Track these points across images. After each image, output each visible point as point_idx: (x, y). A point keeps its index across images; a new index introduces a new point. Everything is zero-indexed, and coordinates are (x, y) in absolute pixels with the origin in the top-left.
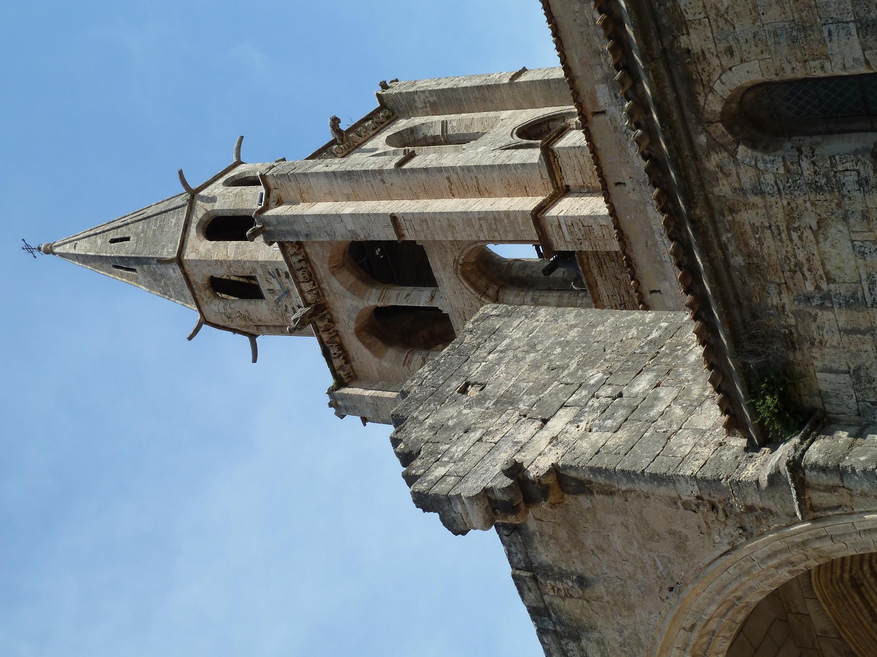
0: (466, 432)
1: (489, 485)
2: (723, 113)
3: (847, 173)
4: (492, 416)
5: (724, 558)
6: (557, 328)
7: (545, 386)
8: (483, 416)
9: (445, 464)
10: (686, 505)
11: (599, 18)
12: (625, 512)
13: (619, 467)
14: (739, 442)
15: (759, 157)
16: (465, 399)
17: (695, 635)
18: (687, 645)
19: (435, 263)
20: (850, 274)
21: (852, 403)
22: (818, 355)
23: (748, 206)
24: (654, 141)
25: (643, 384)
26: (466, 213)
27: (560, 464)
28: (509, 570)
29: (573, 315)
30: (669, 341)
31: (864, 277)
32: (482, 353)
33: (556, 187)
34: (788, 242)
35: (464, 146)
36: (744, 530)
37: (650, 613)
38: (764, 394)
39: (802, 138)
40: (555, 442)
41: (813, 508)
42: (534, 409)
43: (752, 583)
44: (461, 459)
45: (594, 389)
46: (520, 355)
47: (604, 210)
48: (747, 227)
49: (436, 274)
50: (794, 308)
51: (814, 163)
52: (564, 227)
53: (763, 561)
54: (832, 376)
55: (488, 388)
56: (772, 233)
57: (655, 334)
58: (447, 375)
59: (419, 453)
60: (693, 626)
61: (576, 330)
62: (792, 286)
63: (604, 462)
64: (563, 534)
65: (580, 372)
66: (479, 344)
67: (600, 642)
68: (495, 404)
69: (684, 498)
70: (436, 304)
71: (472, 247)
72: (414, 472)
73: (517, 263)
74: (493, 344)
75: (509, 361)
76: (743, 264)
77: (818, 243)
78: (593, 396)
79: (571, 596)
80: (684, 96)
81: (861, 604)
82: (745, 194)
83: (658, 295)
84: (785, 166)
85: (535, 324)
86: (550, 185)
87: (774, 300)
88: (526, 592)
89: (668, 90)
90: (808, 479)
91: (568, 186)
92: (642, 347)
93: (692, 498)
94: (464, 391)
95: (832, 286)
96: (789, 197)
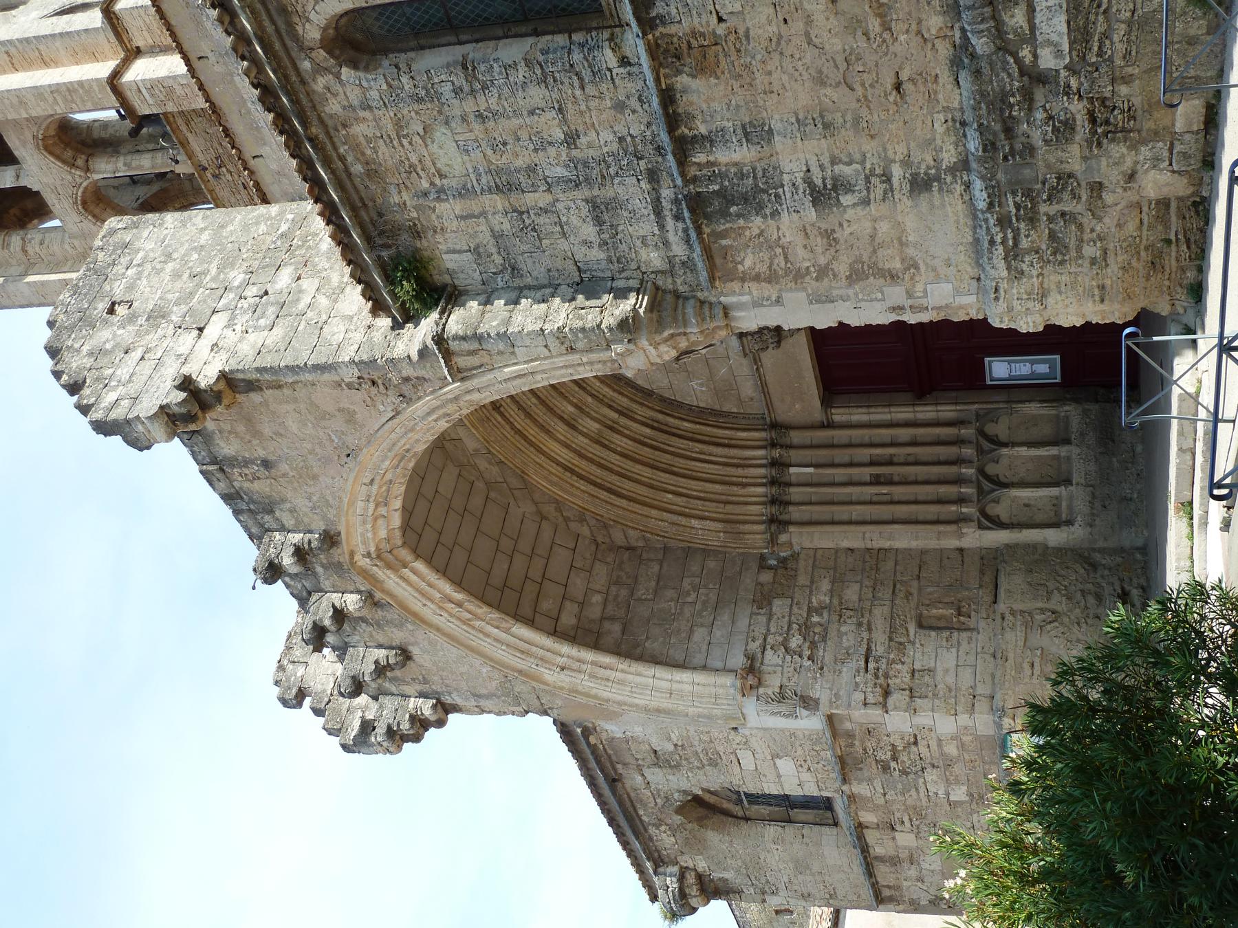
0: (126, 353)
1: (165, 402)
2: (321, 40)
3: (443, 84)
4: (147, 333)
5: (390, 422)
6: (187, 234)
7: (192, 294)
8: (139, 334)
9: (115, 388)
10: (350, 386)
11: (294, 162)
12: (295, 400)
13: (282, 364)
14: (384, 322)
15: (362, 77)
16: (116, 320)
17: (375, 487)
18: (369, 496)
19: (13, 142)
20: (458, 169)
21: (477, 275)
22: (441, 240)
23: (358, 120)
24: (261, 70)
25: (284, 279)
26: (36, 88)
27: (227, 370)
28: (195, 468)
29: (200, 217)
30: (299, 232)
31: (471, 170)
32: (119, 269)
33: (126, 50)
34: (400, 148)
35: (13, 12)
36: (404, 397)
37: (333, 478)
38: (401, 281)
39: (398, 55)
40: (216, 349)
41: (459, 371)
42: (187, 319)
43: (416, 437)
44: (130, 381)
45: (240, 290)
46: (158, 266)
47: (183, 69)
48: (361, 139)
49: (16, 153)
50: (414, 203)
51: (412, 77)
52: (144, 91)
53: (423, 418)
54: (456, 255)
55: (135, 304)
56: (385, 142)
57: (284, 228)
58: (90, 297)
59: (84, 382)
60: (372, 480)
61: (206, 232)
62: (410, 185)
63: (268, 361)
64: (241, 428)
65: (222, 276)
66: (114, 260)
67: (292, 511)
68: (147, 320)
69: (347, 380)
70: (25, 182)
71: (49, 120)
72: (85, 401)
73: (96, 124)
74: (128, 258)
75: (149, 275)
76: (362, 171)
77: (426, 146)
78: (241, 298)
79: (259, 478)
80: (282, 27)
81: (503, 422)
82: (354, 110)
83: (261, 159)
84: (386, 82)
85: (166, 232)
86: (119, 48)
87: (397, 199)
88: (216, 483)
89: (267, 23)
90: (452, 348)
91: (138, 48)
92: (275, 242)
93: (355, 379)
94: (111, 311)
95: (444, 181)
96: (394, 109)
